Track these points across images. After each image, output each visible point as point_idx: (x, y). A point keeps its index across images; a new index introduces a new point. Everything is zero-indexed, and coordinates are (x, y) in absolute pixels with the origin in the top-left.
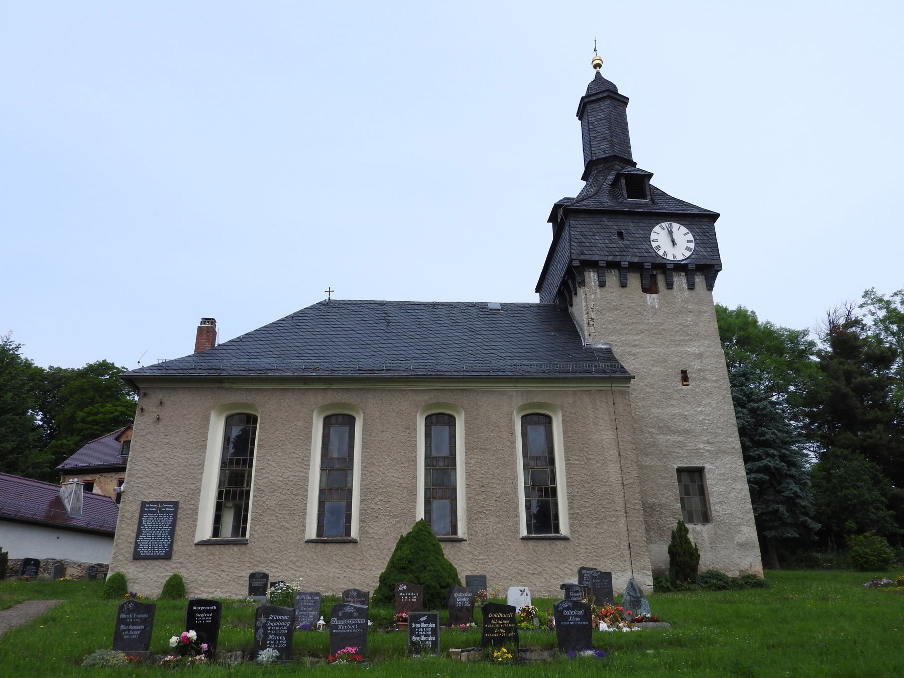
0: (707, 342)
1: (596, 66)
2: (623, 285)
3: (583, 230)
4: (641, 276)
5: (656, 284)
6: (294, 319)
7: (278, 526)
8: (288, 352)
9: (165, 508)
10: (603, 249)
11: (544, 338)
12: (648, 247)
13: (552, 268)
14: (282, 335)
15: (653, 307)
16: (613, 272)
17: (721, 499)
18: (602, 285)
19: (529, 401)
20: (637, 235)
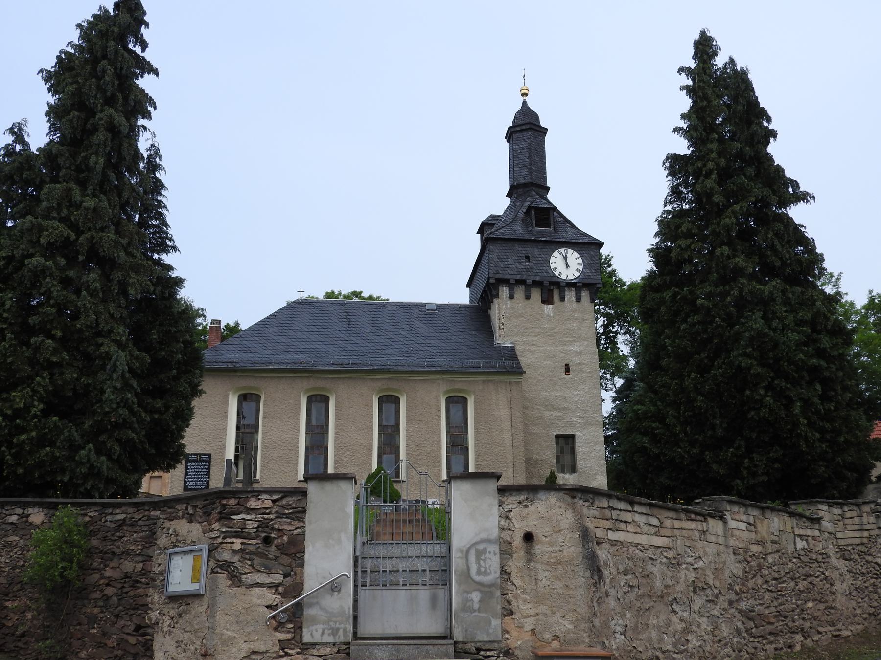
0: (586, 343)
1: (523, 95)
2: (528, 297)
4: (542, 290)
5: (552, 297)
7: (279, 471)
9: (203, 458)
11: (467, 337)
12: (547, 268)
13: (478, 274)
14: (270, 332)
15: (548, 315)
16: (521, 287)
17: (585, 457)
18: (511, 297)
19: (452, 388)
20: (540, 259)
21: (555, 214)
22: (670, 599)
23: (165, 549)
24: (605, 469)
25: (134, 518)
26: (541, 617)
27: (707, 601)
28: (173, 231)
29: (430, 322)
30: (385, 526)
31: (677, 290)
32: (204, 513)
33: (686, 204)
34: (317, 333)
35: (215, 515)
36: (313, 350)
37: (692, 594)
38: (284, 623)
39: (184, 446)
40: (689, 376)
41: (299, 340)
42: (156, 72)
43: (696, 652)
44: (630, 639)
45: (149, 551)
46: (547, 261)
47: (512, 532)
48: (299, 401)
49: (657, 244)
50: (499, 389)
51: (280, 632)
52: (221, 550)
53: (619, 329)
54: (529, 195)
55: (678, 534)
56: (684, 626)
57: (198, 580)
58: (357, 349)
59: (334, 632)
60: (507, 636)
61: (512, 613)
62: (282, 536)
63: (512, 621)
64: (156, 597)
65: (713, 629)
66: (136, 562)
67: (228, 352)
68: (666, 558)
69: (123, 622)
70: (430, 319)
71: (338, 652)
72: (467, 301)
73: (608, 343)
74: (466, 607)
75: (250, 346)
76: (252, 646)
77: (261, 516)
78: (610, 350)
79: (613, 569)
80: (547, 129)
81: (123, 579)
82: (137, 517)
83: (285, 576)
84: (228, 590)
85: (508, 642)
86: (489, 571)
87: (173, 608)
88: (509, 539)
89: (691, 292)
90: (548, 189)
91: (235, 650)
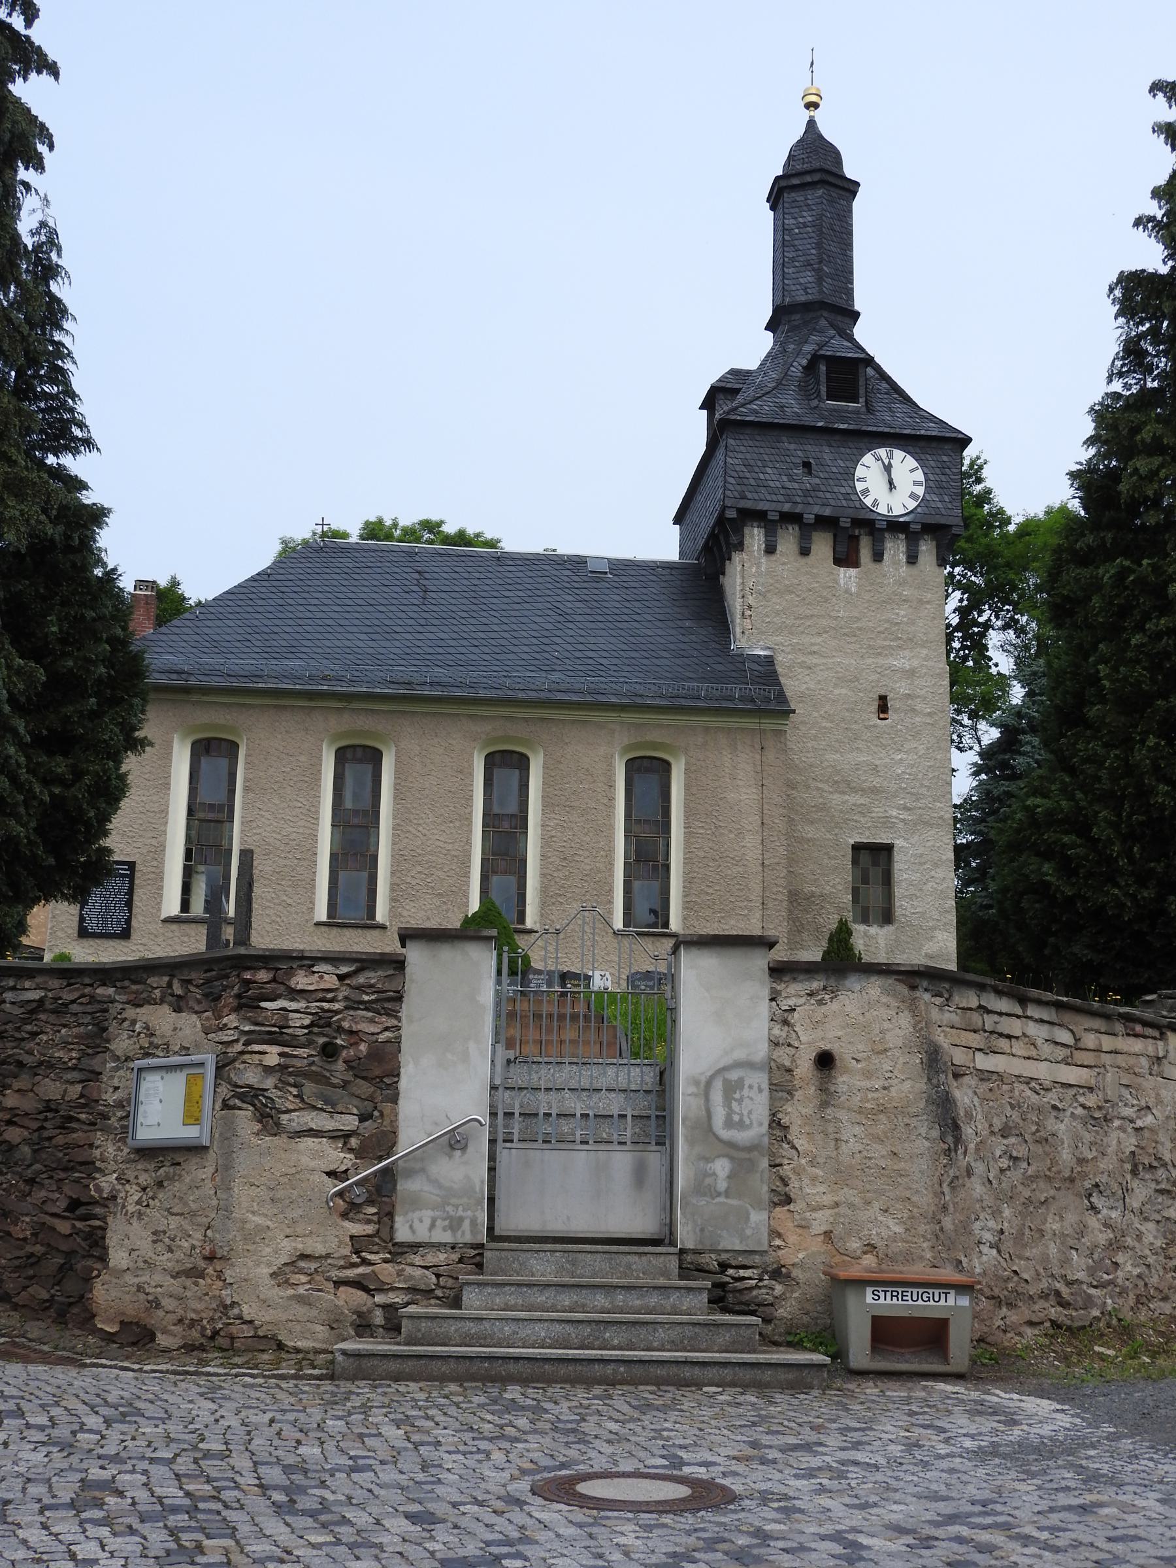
0: (925, 652)
1: (808, 106)
2: (805, 552)
3: (748, 457)
4: (835, 536)
5: (857, 552)
6: (271, 578)
8: (275, 643)
10: (776, 491)
12: (849, 490)
13: (699, 498)
14: (260, 609)
15: (847, 591)
16: (790, 528)
17: (912, 891)
18: (770, 550)
19: (639, 739)
20: (834, 470)
21: (870, 371)
22: (1087, 1184)
23: (126, 1060)
24: (952, 917)
25: (60, 998)
26: (842, 1210)
27: (1157, 1191)
28: (86, 408)
29: (595, 598)
30: (524, 1026)
31: (1127, 563)
32: (206, 995)
33: (1153, 380)
34: (357, 615)
35: (228, 999)
36: (348, 650)
37: (1129, 1177)
38: (360, 1204)
39: (108, 851)
40: (1143, 742)
41: (320, 629)
42: (53, 70)
43: (1131, 1286)
44: (1007, 1256)
45: (95, 1061)
46: (850, 475)
47: (793, 1051)
48: (320, 759)
49: (1090, 461)
50: (740, 748)
51: (352, 1220)
52: (242, 1066)
53: (993, 618)
54: (814, 329)
55: (1108, 1063)
56: (1111, 1236)
57: (197, 1120)
58: (440, 650)
59: (455, 1224)
60: (778, 1242)
61: (788, 1200)
62: (356, 1044)
63: (788, 1215)
64: (111, 1149)
65: (1167, 1244)
66: (67, 1082)
67: (171, 650)
68: (1083, 1106)
69: (43, 1193)
70: (596, 591)
71: (461, 1261)
72: (671, 553)
73: (966, 647)
74: (702, 1187)
75: (217, 638)
76: (300, 1246)
77: (318, 1004)
78: (970, 663)
79: (982, 1126)
80: (857, 184)
81: (40, 1113)
82: (67, 996)
83: (363, 1118)
84: (255, 1141)
85: (780, 1253)
86: (748, 1122)
87: (146, 1171)
88: (787, 1063)
89: (1155, 568)
90: (856, 315)
91: (268, 1250)
